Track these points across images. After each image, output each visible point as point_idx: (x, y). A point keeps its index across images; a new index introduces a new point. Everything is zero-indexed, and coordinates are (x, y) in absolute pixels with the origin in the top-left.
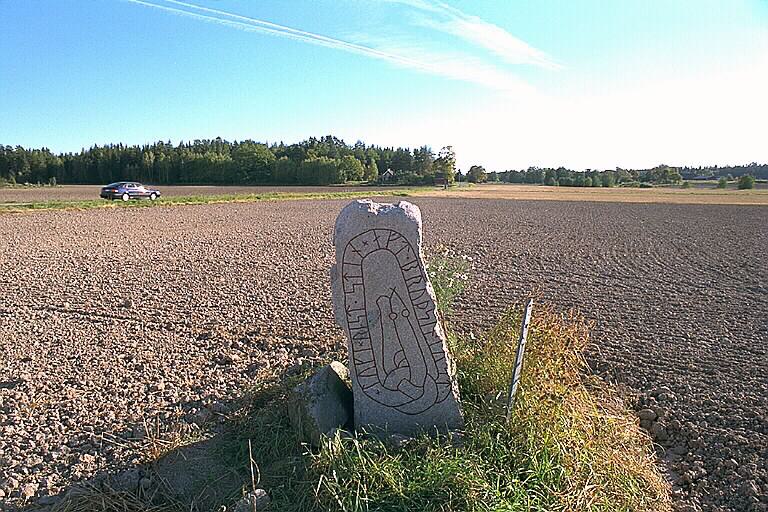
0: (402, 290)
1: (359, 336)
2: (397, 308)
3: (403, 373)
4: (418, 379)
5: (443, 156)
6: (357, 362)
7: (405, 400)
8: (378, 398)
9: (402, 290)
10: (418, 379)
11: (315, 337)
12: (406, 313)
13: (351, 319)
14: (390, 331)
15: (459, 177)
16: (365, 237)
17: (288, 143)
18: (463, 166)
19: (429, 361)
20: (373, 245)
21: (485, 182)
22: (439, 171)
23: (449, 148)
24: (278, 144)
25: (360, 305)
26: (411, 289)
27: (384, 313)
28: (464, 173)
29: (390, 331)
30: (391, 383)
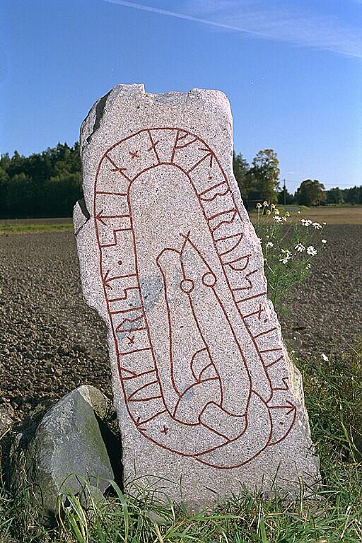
0: (201, 237)
1: (127, 326)
2: (195, 270)
3: (208, 391)
4: (235, 401)
5: (259, 164)
6: (125, 374)
7: (211, 440)
8: (167, 440)
9: (201, 237)
10: (236, 397)
11: (61, 387)
12: (210, 279)
13: (113, 294)
14: (182, 312)
15: (284, 199)
16: (133, 145)
17: (26, 153)
18: (290, 181)
19: (256, 368)
20: (147, 159)
21: (323, 204)
22: (255, 190)
23: (268, 152)
24: (11, 156)
25: (127, 268)
26: (219, 234)
27: (171, 280)
28: (292, 191)
29: (182, 312)
30: (187, 411)
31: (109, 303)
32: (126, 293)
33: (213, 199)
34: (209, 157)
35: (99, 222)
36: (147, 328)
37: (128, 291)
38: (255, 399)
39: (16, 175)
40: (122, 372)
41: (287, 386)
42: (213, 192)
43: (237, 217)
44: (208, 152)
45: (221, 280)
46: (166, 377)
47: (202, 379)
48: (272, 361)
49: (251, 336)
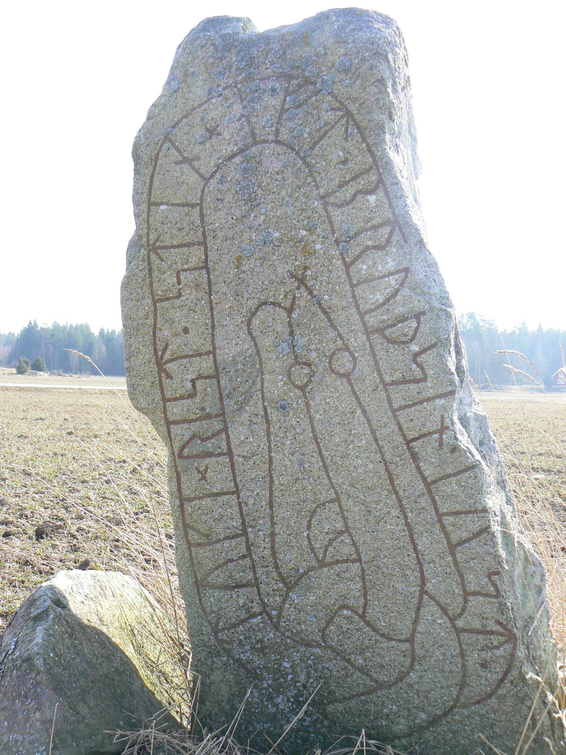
19: (430, 543)
31: (193, 549)
32: (194, 386)
33: (351, 201)
34: (344, 121)
35: (153, 257)
36: (230, 453)
37: (198, 383)
38: (430, 611)
39: (379, 692)
40: (190, 532)
41: (497, 590)
42: (349, 191)
43: (397, 236)
44: (339, 113)
45: (365, 364)
46: (262, 549)
47: (328, 559)
48: (465, 535)
49: (424, 479)
